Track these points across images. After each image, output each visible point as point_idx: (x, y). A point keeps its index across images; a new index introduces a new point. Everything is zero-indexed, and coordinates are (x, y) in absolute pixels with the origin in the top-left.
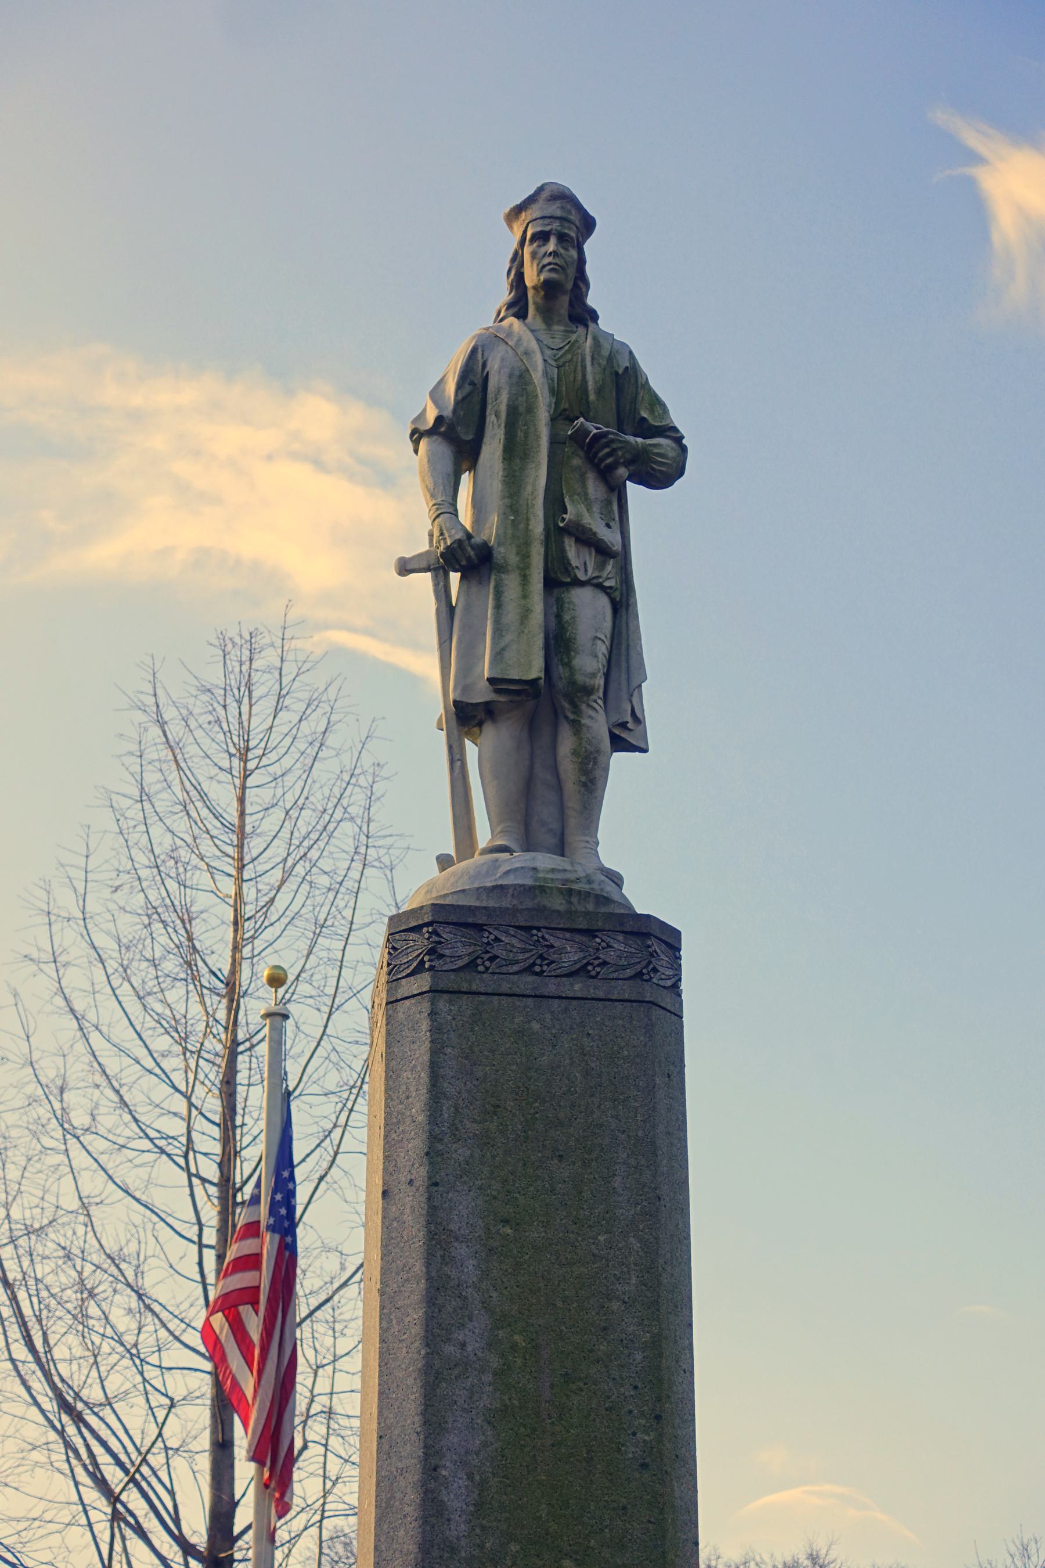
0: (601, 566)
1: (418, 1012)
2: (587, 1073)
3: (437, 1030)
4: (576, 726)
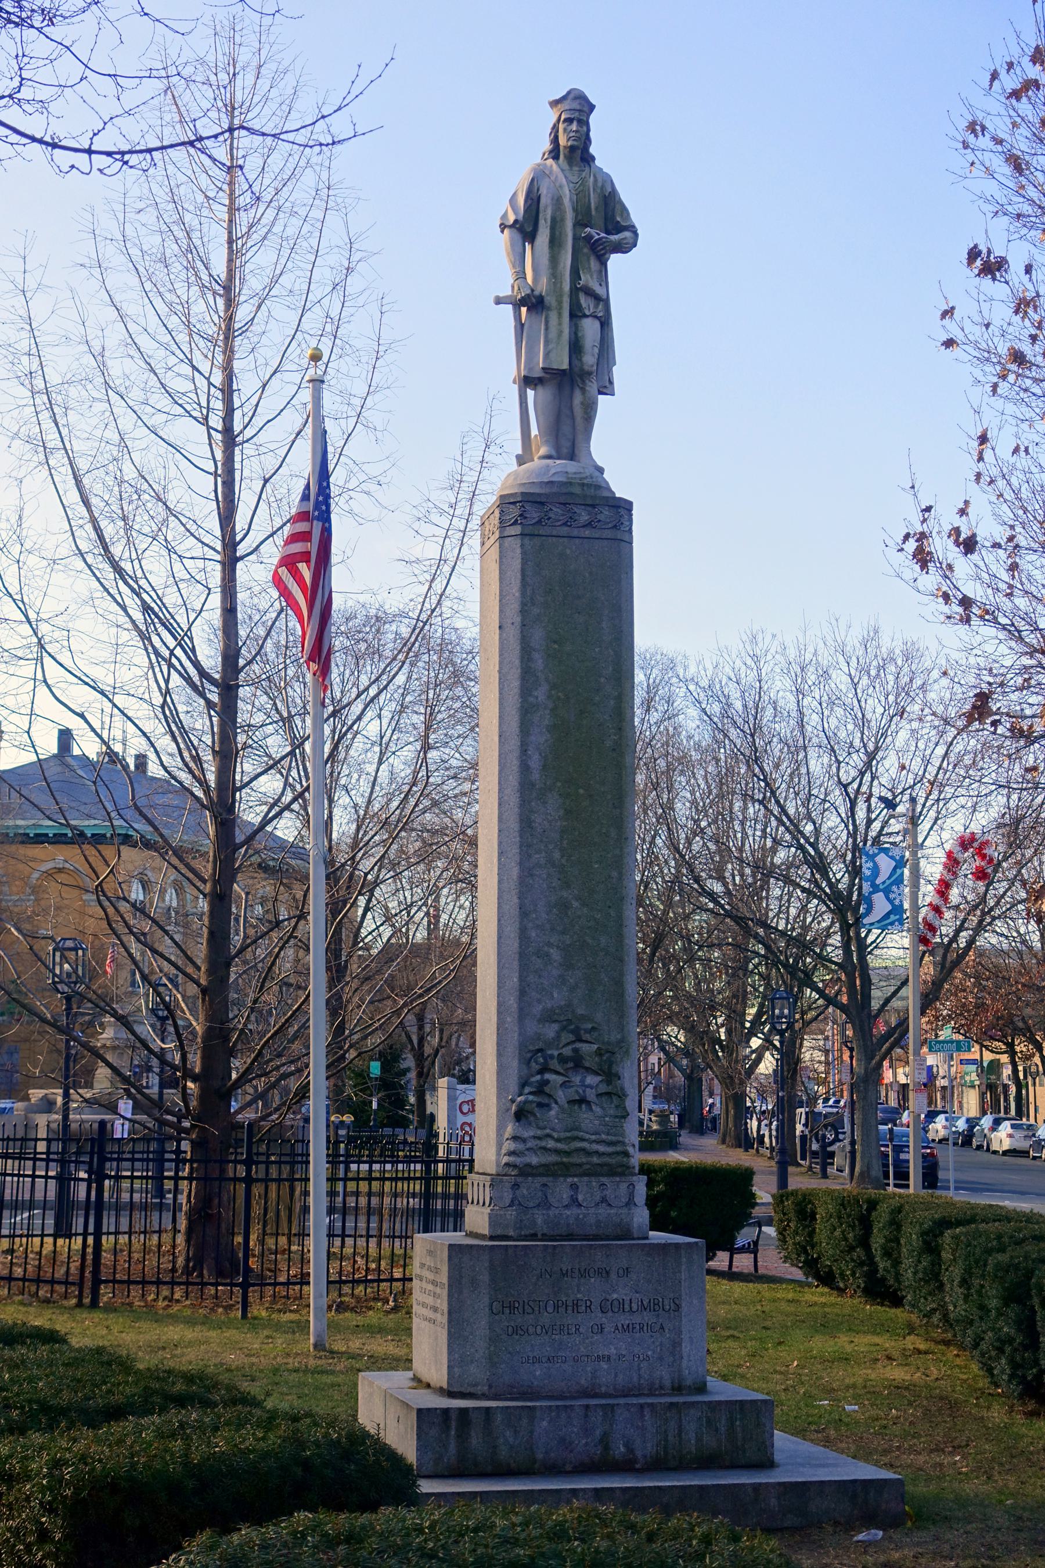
0: (596, 306)
1: (515, 544)
2: (591, 573)
3: (524, 553)
4: (583, 390)
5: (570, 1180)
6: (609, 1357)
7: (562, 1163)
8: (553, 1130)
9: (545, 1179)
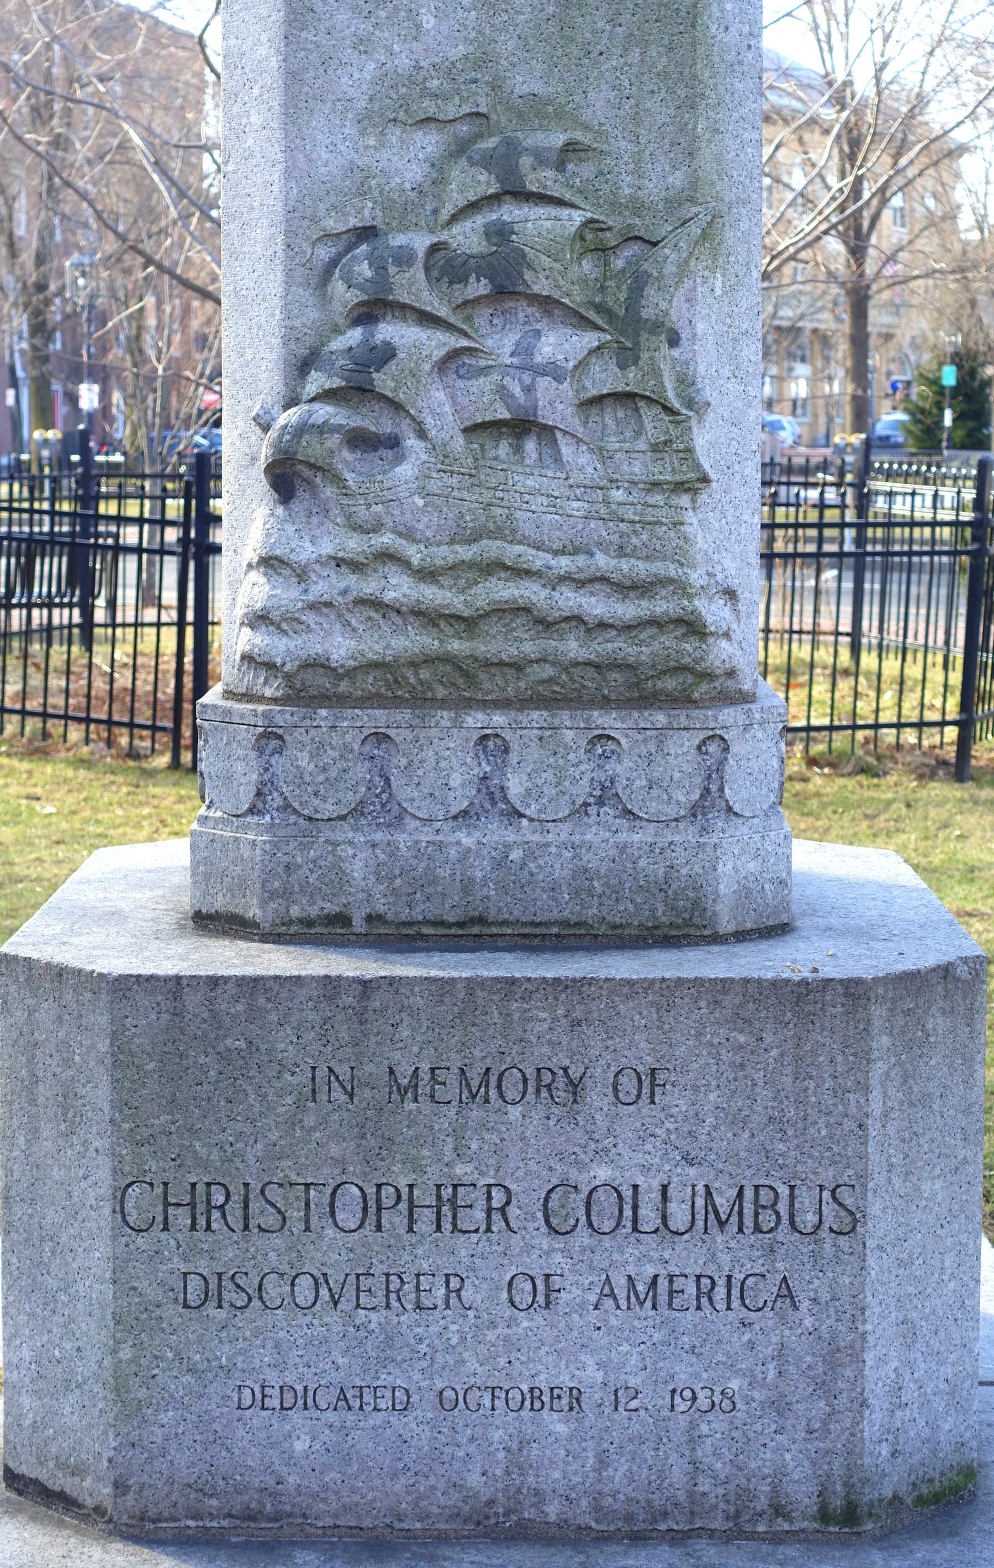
5: (475, 720)
6: (576, 1396)
7: (447, 659)
8: (408, 534)
9: (378, 718)
